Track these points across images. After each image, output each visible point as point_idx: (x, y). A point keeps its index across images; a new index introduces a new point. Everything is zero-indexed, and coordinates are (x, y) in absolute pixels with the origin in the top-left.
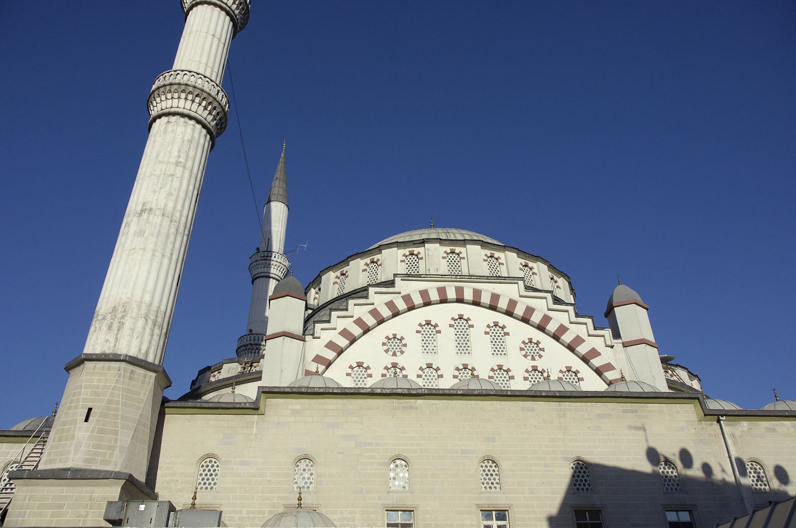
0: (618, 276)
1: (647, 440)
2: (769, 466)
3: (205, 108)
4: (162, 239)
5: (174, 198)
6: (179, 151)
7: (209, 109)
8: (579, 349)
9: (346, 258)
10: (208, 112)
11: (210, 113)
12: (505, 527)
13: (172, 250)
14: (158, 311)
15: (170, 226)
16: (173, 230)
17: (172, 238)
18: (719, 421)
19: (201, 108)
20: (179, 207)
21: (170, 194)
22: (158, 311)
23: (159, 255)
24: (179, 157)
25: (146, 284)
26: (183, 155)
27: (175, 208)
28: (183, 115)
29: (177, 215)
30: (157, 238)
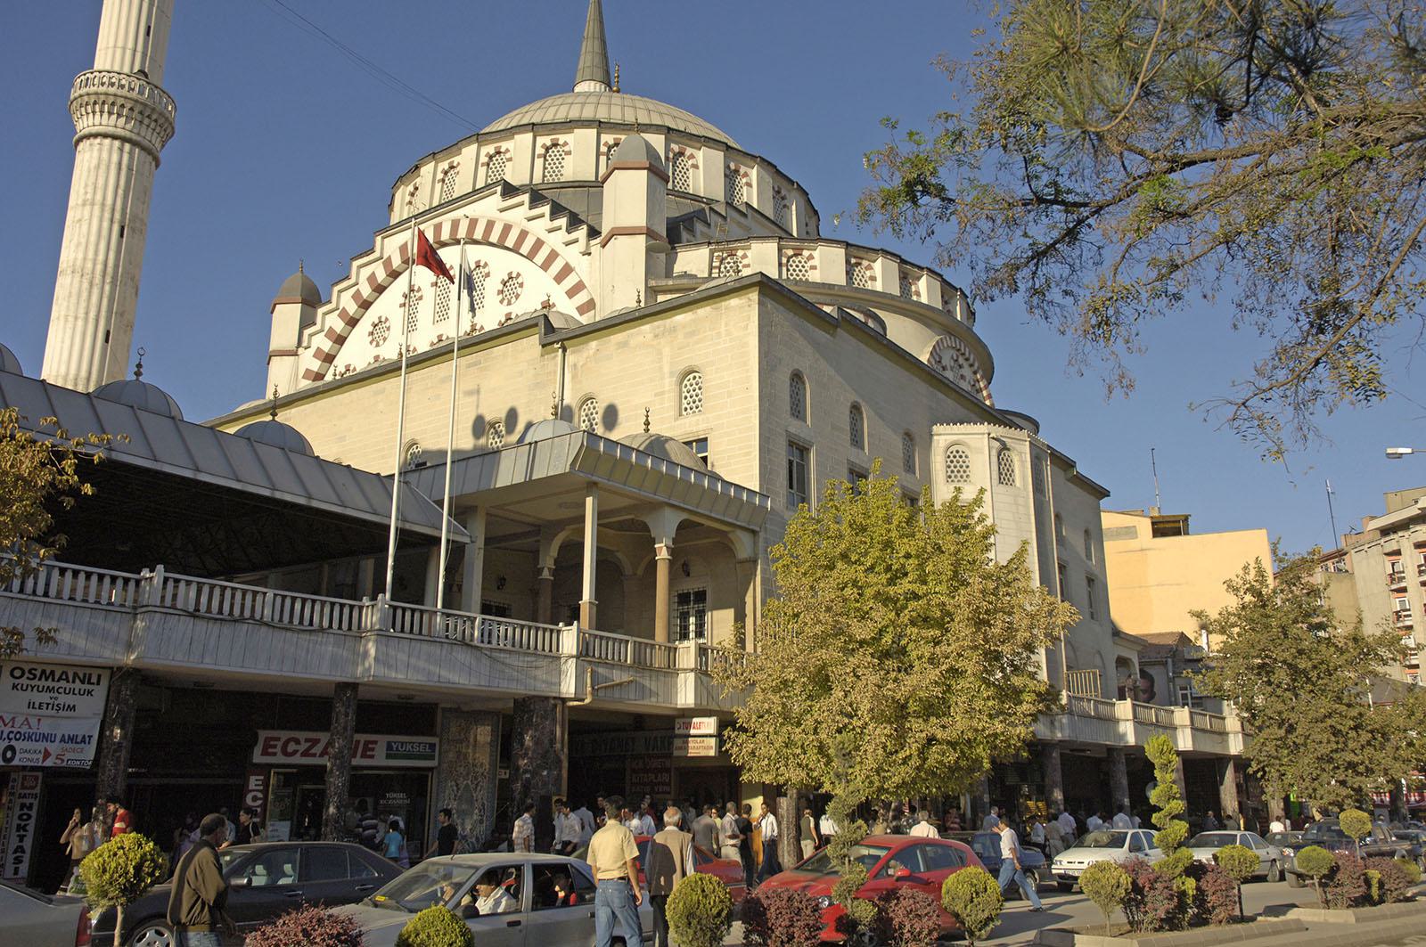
0: (1311, 468)
1: (478, 406)
2: (998, 300)
3: (110, 113)
4: (74, 300)
5: (82, 248)
6: (86, 186)
7: (89, 111)
8: (1033, 183)
9: (879, 248)
10: (115, 116)
11: (119, 115)
12: (497, 598)
13: (88, 307)
14: (76, 379)
15: (81, 282)
16: (86, 285)
17: (85, 295)
18: (261, 618)
19: (105, 115)
20: (91, 255)
21: (79, 244)
22: (76, 379)
23: (71, 319)
24: (86, 193)
25: (61, 355)
26: (90, 190)
27: (85, 259)
28: (95, 136)
29: (89, 265)
30: (69, 302)
